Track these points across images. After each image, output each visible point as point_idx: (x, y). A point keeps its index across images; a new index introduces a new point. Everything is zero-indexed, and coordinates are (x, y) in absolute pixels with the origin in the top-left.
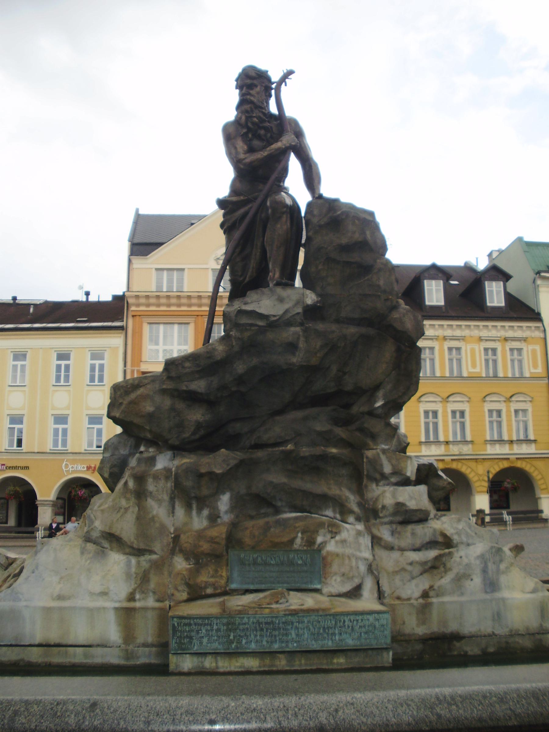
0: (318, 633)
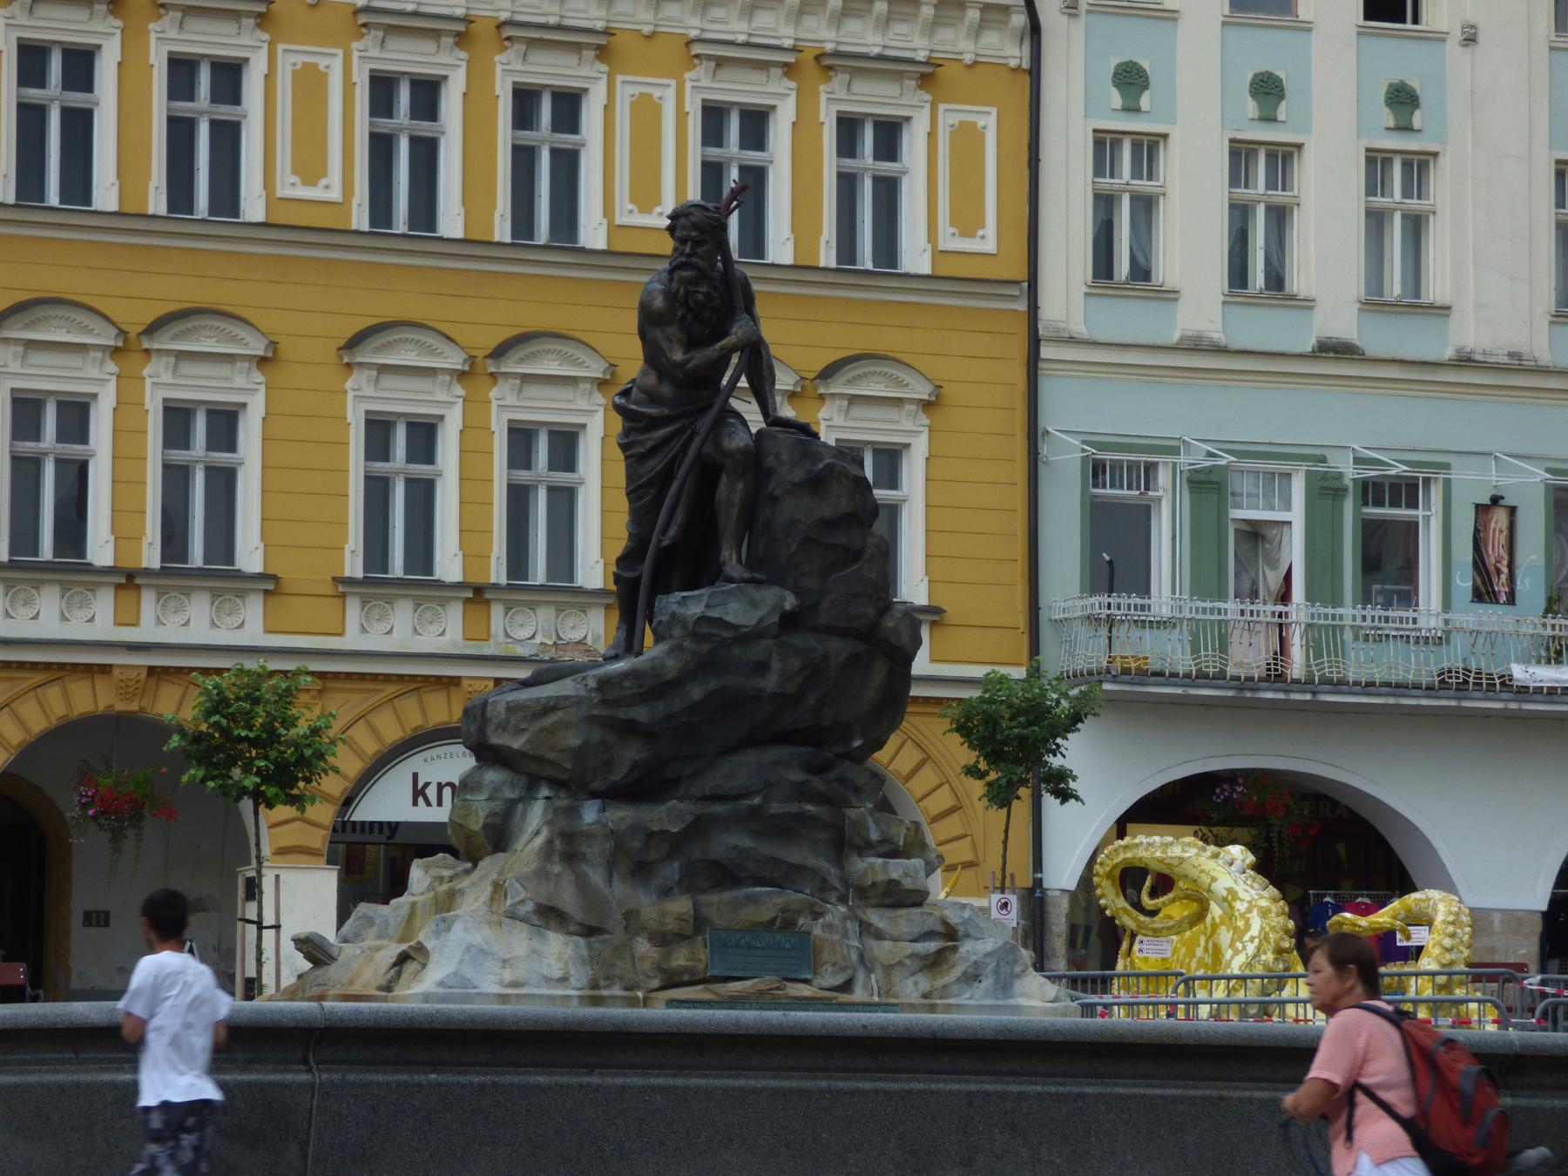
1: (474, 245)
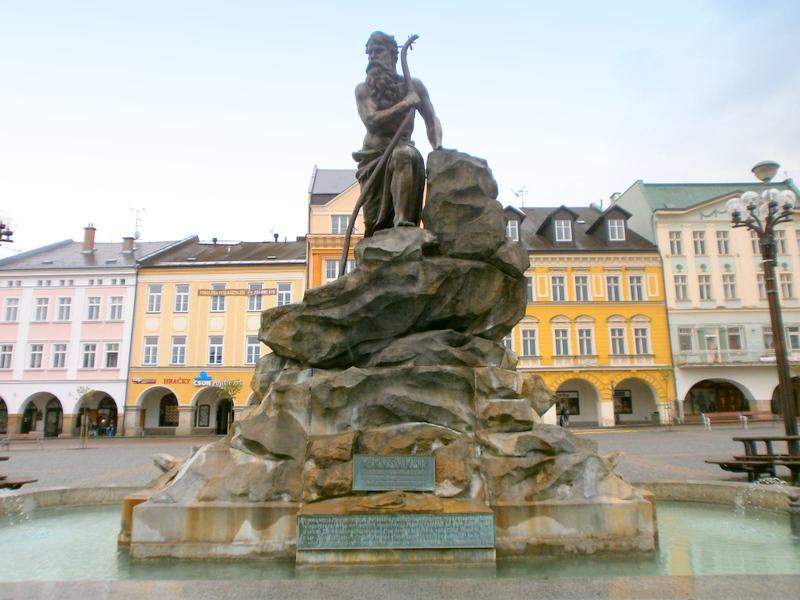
0: (429, 533)
1: (570, 302)
